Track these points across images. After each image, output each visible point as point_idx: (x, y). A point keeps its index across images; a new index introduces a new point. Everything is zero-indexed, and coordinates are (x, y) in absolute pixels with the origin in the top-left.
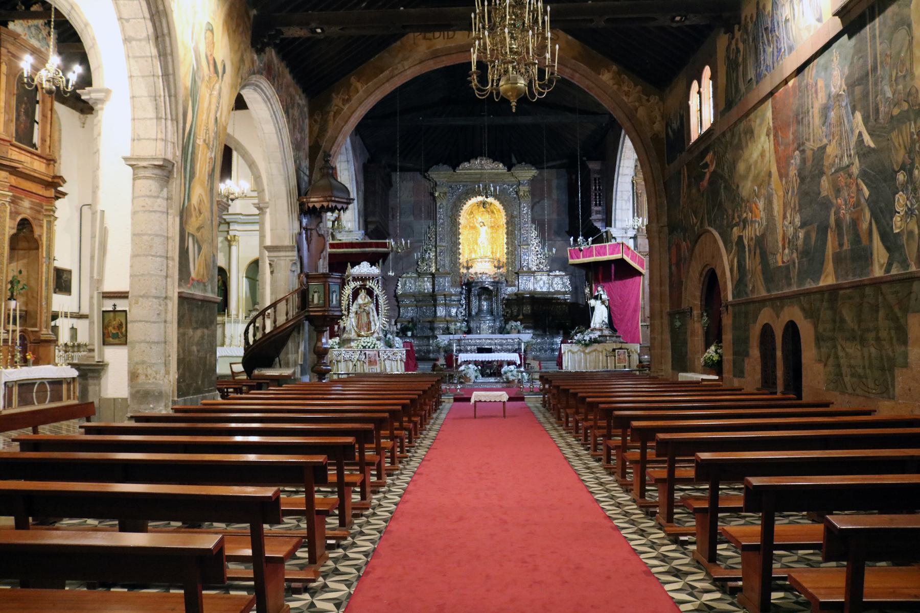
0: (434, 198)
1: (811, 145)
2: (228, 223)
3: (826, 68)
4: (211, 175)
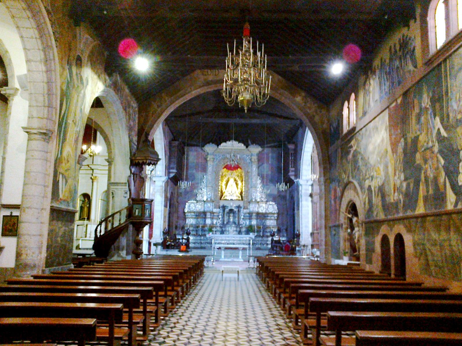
0: (207, 160)
2: (93, 170)
4: (76, 141)
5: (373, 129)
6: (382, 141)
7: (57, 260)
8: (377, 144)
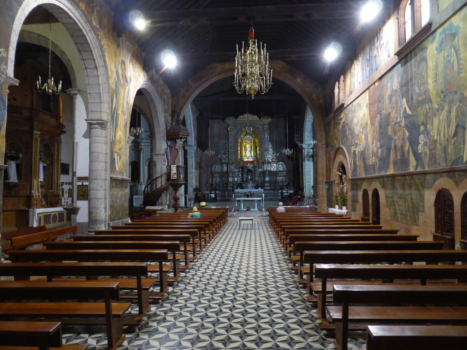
0: (228, 131)
1: (384, 112)
3: (391, 78)
5: (357, 106)
6: (364, 115)
7: (118, 216)
8: (360, 118)
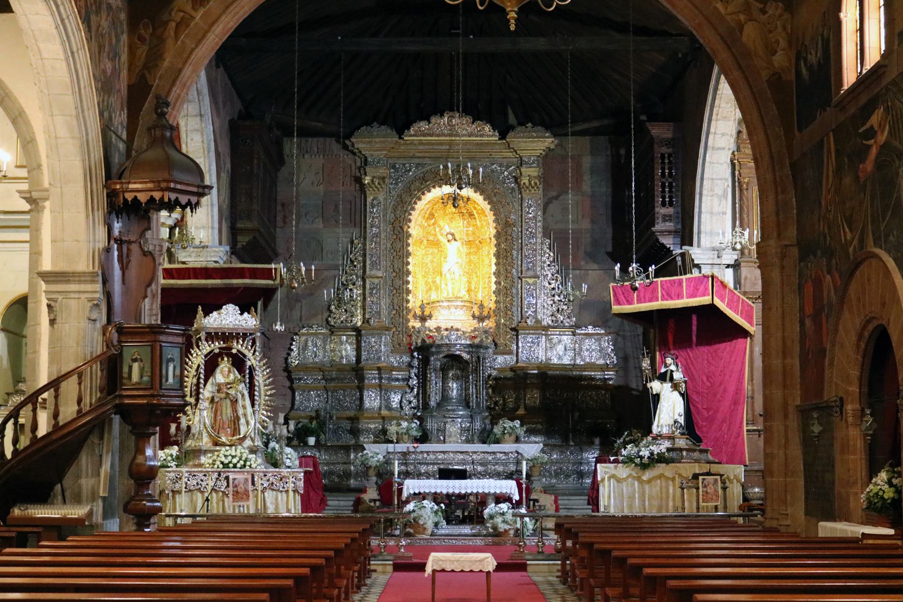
0: (362, 188)
